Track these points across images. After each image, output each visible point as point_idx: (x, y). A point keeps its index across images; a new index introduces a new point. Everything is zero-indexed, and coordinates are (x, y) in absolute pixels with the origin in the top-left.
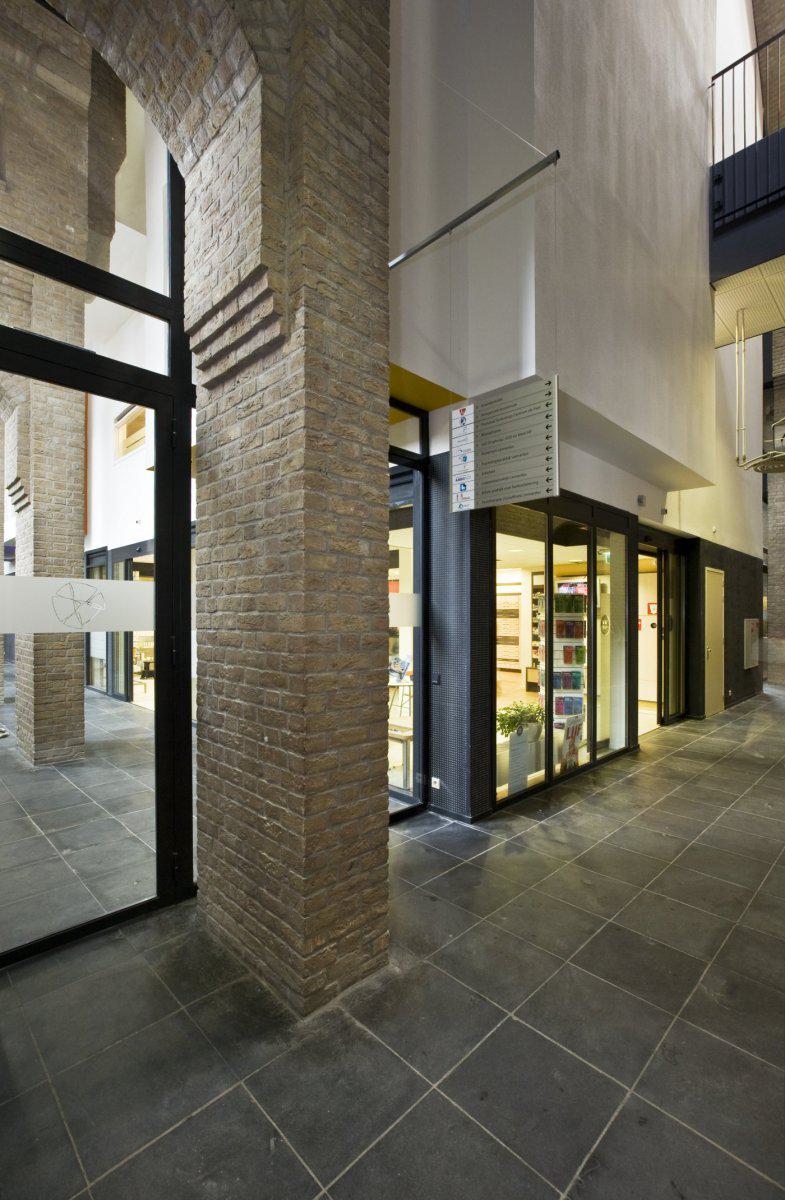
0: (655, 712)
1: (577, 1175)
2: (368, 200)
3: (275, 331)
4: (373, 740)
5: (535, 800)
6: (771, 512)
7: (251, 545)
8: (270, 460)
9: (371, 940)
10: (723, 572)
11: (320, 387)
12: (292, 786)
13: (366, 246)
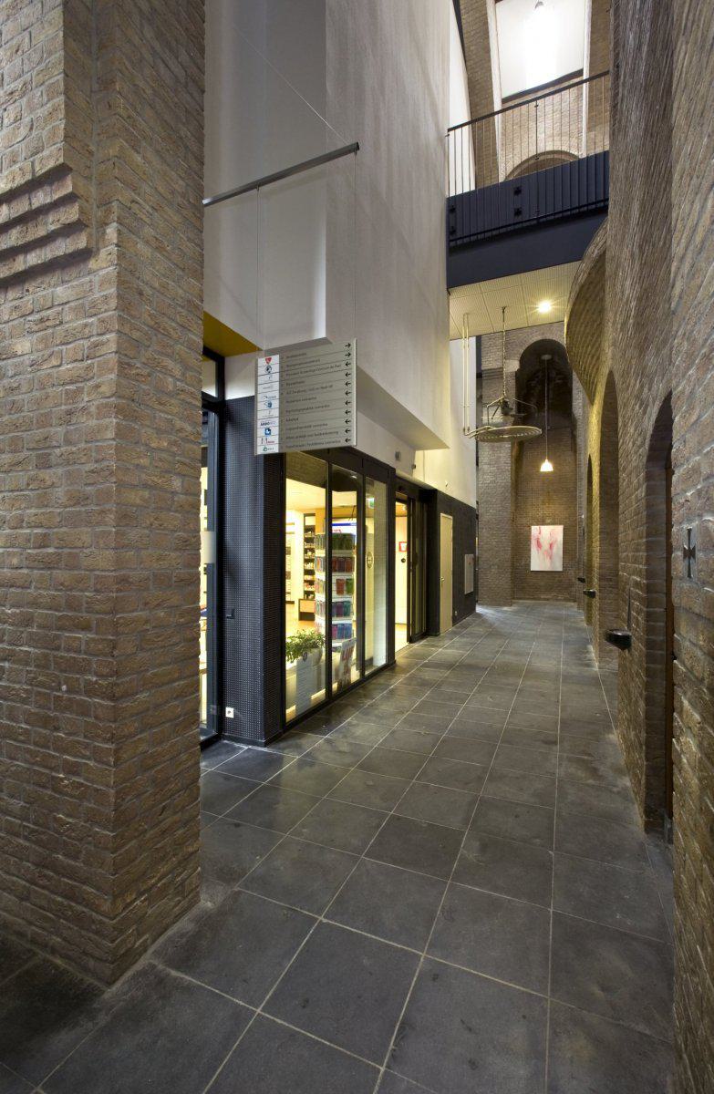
0: (406, 630)
1: (391, 1046)
2: (184, 131)
3: (81, 242)
4: (185, 678)
5: (321, 716)
6: (480, 473)
7: (46, 475)
8: (71, 382)
9: (184, 881)
10: (451, 517)
11: (133, 312)
12: (99, 736)
13: (182, 179)
